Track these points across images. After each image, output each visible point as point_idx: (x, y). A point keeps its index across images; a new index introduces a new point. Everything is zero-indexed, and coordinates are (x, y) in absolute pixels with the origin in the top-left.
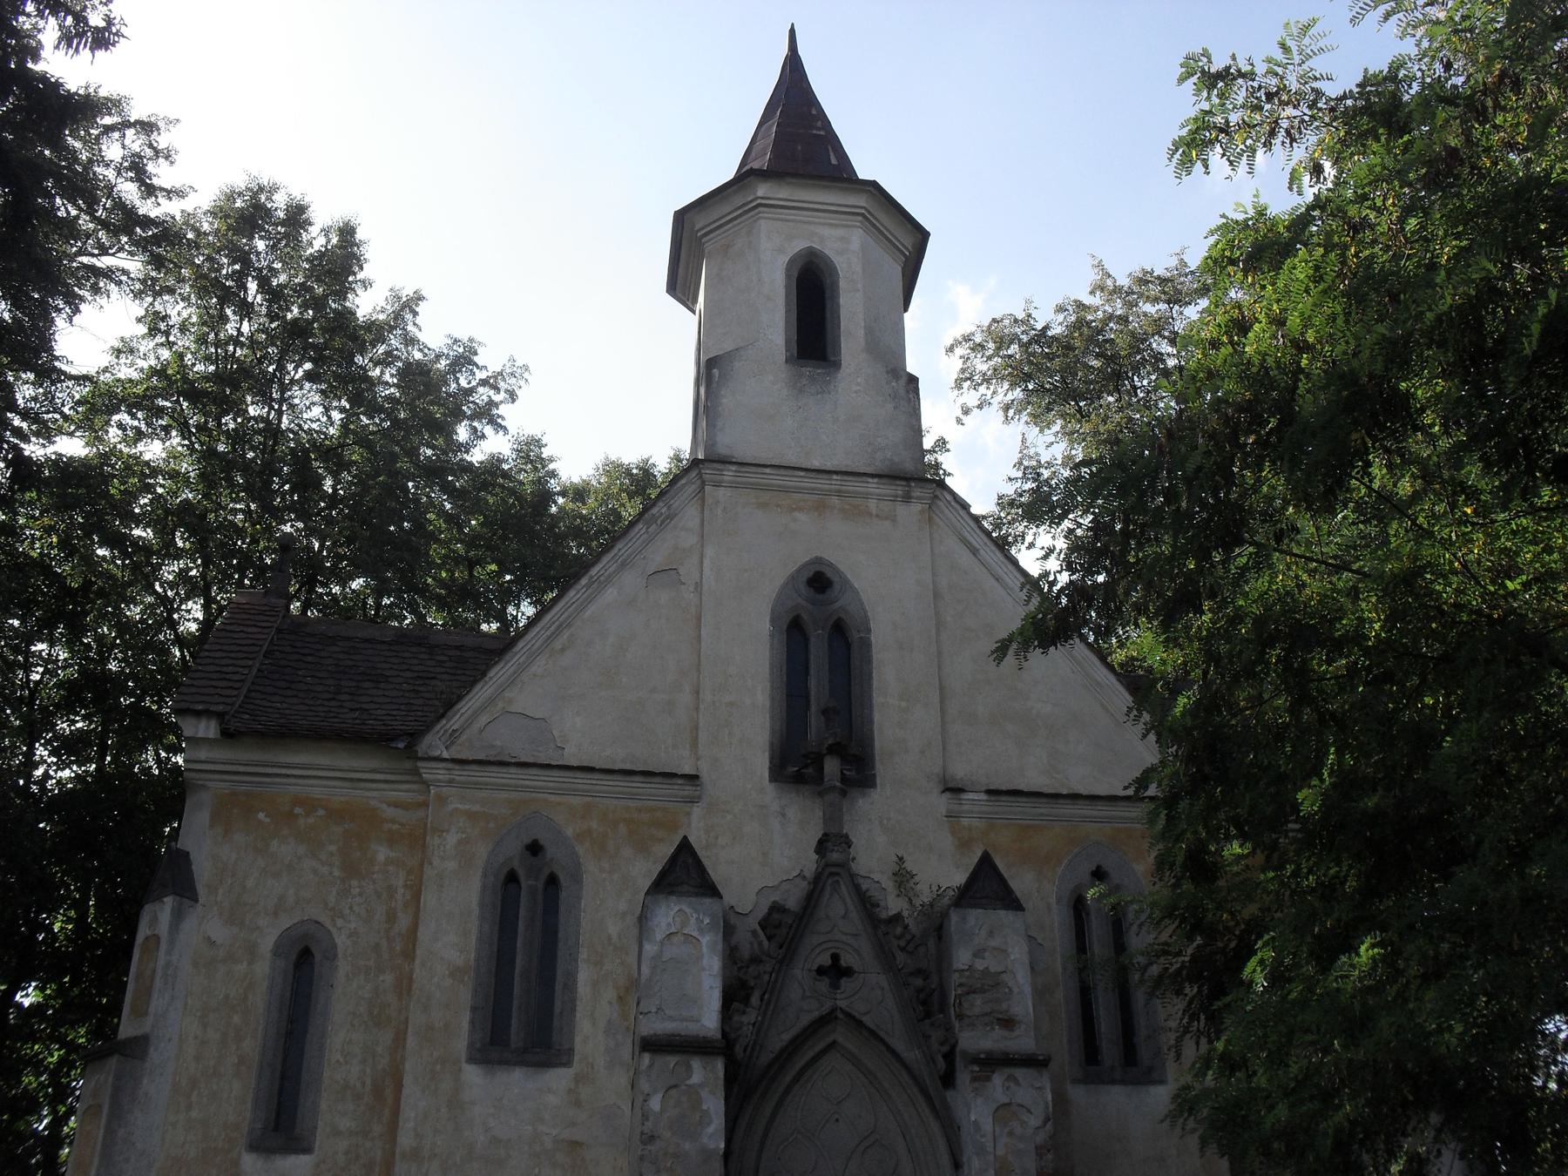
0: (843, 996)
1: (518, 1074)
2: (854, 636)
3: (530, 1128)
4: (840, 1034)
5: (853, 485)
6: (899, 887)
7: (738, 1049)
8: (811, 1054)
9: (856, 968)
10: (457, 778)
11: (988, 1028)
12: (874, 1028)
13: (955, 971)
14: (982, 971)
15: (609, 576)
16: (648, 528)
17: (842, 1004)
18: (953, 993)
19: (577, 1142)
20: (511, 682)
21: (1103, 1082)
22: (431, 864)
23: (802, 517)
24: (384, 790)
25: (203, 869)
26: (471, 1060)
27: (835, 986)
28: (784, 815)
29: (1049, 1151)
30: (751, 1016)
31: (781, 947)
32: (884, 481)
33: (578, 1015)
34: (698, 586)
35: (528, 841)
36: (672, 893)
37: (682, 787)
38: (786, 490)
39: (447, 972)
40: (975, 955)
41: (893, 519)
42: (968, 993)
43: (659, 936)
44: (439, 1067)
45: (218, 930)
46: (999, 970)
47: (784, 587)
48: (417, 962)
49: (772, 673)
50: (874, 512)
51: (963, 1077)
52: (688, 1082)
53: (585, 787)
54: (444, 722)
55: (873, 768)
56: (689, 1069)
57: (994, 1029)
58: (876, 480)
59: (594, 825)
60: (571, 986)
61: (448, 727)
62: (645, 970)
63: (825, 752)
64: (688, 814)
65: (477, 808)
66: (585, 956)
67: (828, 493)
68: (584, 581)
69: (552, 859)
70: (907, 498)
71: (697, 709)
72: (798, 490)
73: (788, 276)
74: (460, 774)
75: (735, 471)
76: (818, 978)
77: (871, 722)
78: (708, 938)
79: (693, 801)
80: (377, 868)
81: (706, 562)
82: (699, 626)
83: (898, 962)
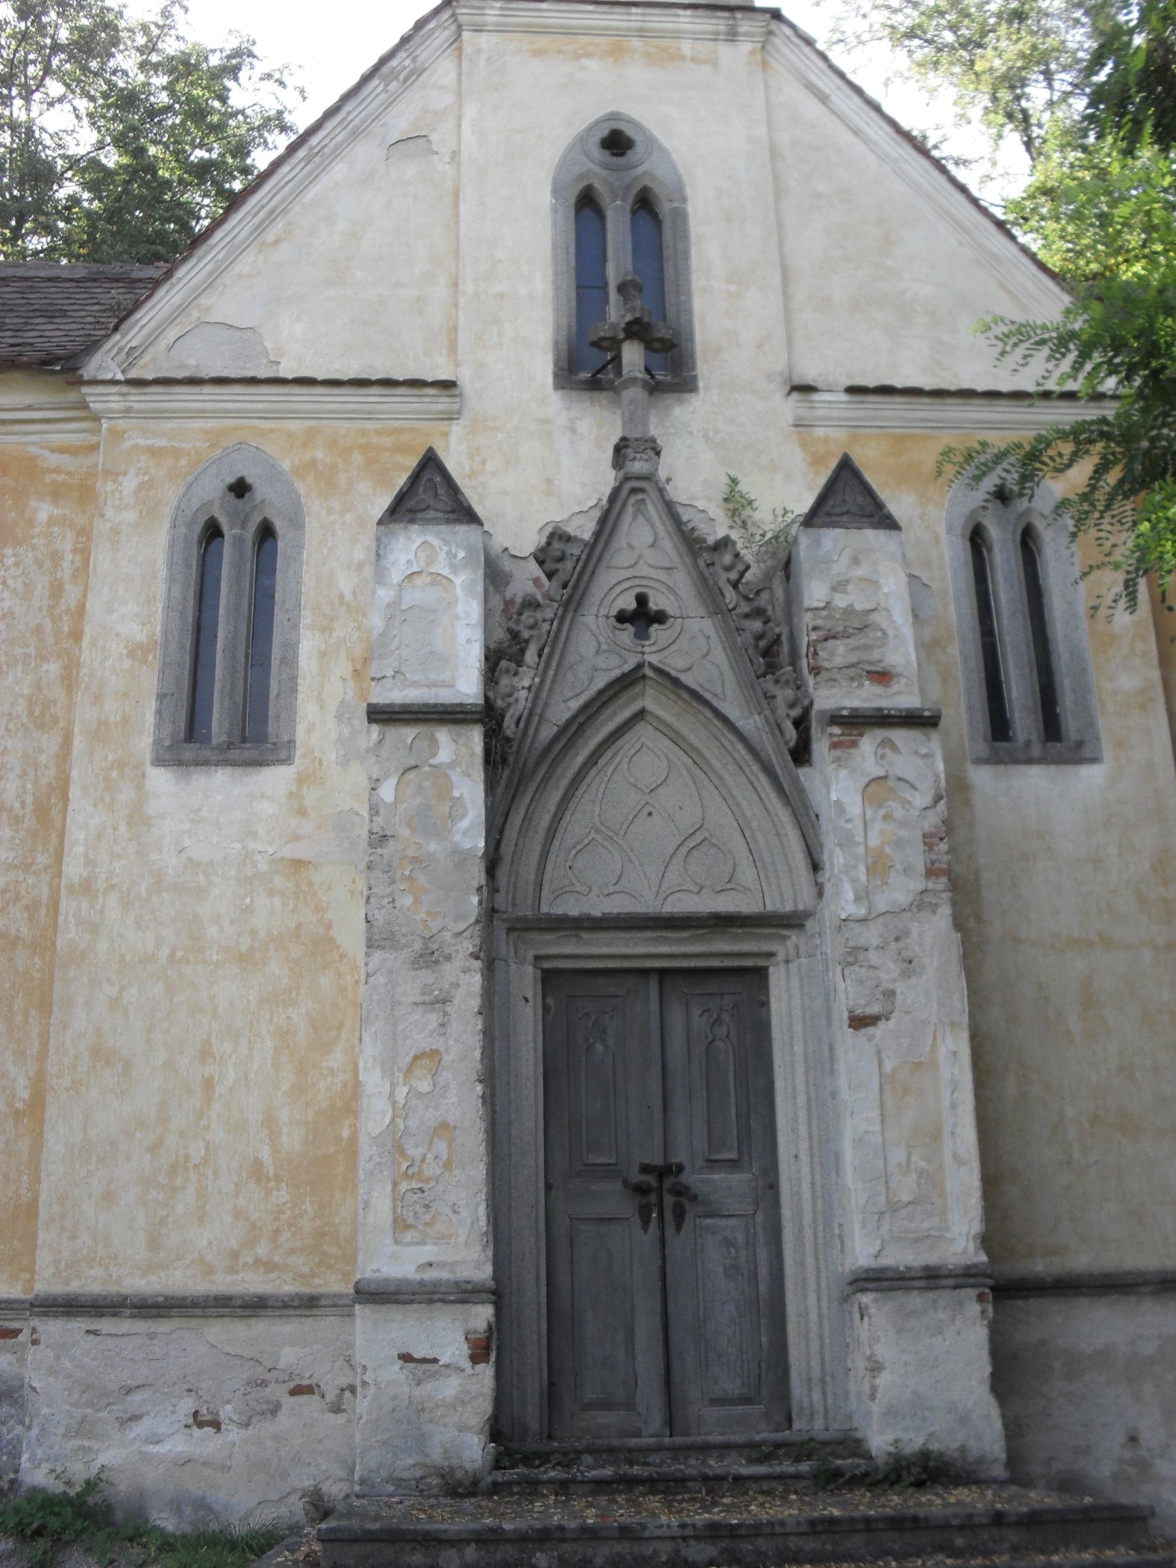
0: (654, 649)
1: (221, 777)
2: (665, 208)
3: (238, 846)
4: (651, 699)
6: (733, 515)
7: (509, 723)
8: (611, 726)
9: (670, 612)
10: (135, 405)
11: (856, 684)
12: (698, 689)
13: (808, 610)
14: (845, 609)
15: (337, 147)
16: (386, 86)
17: (654, 659)
18: (806, 639)
19: (300, 861)
20: (210, 284)
21: (1016, 762)
22: (102, 516)
23: (593, 64)
24: (46, 432)
26: (158, 762)
27: (642, 635)
28: (574, 431)
29: (942, 839)
30: (526, 679)
31: (565, 587)
32: (700, 12)
33: (300, 697)
34: (455, 155)
35: (231, 479)
36: (412, 521)
37: (435, 399)
38: (570, 32)
39: (125, 652)
40: (834, 589)
41: (713, 62)
42: (826, 640)
43: (396, 577)
44: (115, 774)
46: (869, 607)
47: (570, 149)
48: (85, 642)
49: (555, 257)
50: (689, 56)
51: (820, 747)
52: (432, 762)
53: (307, 406)
54: (117, 337)
55: (694, 368)
56: (434, 744)
57: (863, 685)
58: (689, 12)
59: (320, 455)
60: (290, 661)
61: (123, 343)
63: (621, 335)
64: (446, 435)
65: (163, 442)
66: (309, 621)
67: (626, 34)
69: (262, 502)
70: (732, 36)
71: (456, 305)
72: (587, 31)
74: (139, 400)
75: (502, 9)
76: (618, 625)
77: (690, 311)
78: (463, 577)
80: (37, 530)
81: (465, 123)
82: (456, 205)
83: (727, 601)
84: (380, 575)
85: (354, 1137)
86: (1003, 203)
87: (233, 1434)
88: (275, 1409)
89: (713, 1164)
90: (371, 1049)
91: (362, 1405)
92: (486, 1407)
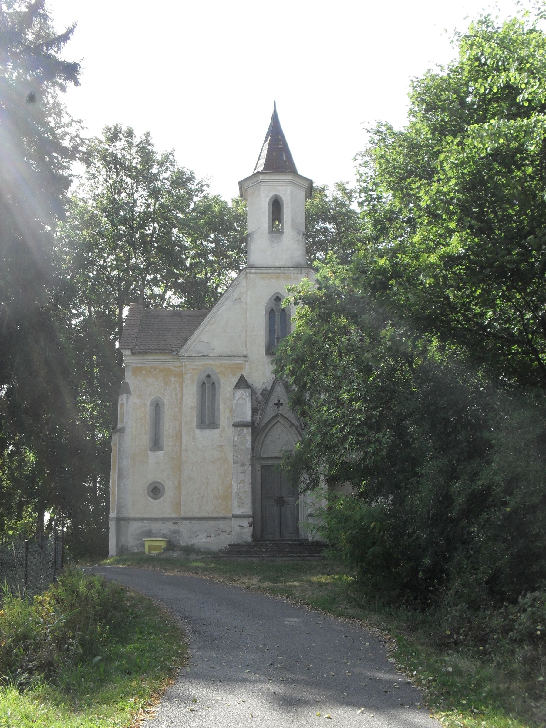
4: (280, 419)
5: (286, 270)
23: (273, 280)
25: (131, 386)
26: (197, 428)
30: (259, 416)
34: (246, 303)
43: (237, 399)
45: (137, 401)
56: (243, 430)
59: (223, 369)
60: (219, 409)
62: (234, 407)
65: (194, 367)
68: (217, 305)
70: (301, 272)
73: (269, 205)
74: (189, 359)
79: (246, 361)
84: (234, 398)
85: (231, 492)
86: (539, 17)
87: (213, 538)
88: (219, 534)
89: (289, 497)
90: (234, 480)
91: (233, 533)
92: (251, 533)
